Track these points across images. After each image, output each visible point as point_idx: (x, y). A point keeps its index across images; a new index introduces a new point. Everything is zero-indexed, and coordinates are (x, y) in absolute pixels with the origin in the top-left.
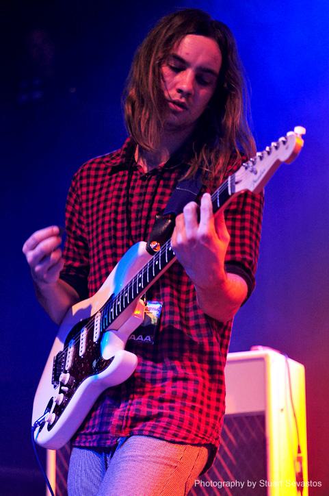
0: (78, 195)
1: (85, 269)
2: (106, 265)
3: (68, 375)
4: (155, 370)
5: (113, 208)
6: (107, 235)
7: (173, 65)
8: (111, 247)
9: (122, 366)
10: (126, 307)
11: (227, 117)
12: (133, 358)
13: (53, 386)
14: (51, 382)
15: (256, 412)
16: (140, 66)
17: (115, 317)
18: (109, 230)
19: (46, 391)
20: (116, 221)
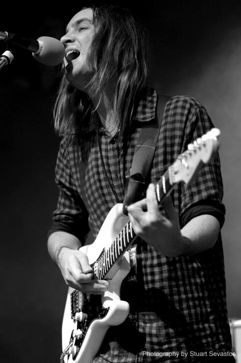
0: (68, 161)
1: (84, 214)
2: (99, 217)
3: (81, 313)
4: (145, 116)
5: (95, 170)
6: (96, 195)
7: (154, 162)
8: (100, 197)
9: (118, 312)
10: (115, 260)
11: (136, 86)
12: (125, 305)
13: (73, 320)
14: (70, 317)
15: (197, 233)
16: (142, 82)
17: (111, 266)
18: (97, 190)
19: (69, 327)
20: (100, 181)
